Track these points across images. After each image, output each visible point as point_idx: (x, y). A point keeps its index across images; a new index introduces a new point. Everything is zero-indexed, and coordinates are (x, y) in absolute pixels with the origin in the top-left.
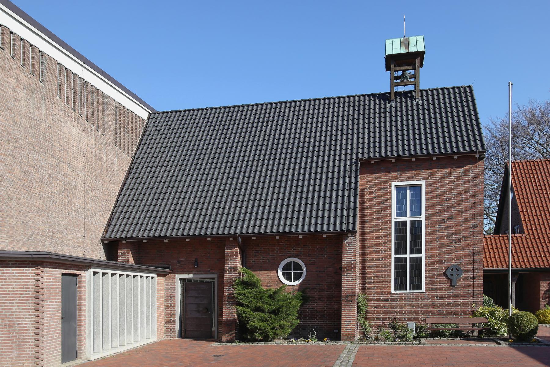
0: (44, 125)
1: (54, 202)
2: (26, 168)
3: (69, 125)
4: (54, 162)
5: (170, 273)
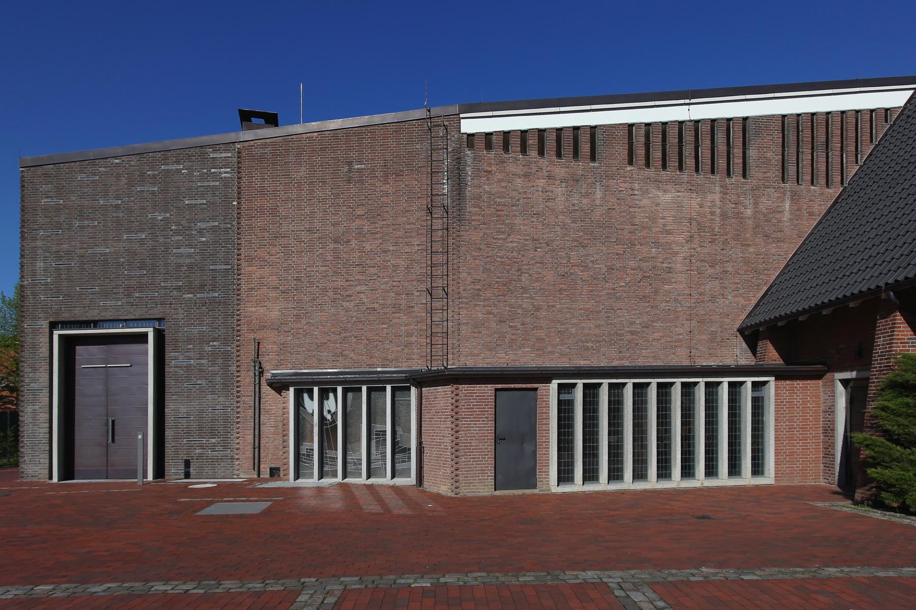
0: (598, 213)
1: (618, 299)
2: (562, 270)
3: (654, 192)
5: (826, 372)
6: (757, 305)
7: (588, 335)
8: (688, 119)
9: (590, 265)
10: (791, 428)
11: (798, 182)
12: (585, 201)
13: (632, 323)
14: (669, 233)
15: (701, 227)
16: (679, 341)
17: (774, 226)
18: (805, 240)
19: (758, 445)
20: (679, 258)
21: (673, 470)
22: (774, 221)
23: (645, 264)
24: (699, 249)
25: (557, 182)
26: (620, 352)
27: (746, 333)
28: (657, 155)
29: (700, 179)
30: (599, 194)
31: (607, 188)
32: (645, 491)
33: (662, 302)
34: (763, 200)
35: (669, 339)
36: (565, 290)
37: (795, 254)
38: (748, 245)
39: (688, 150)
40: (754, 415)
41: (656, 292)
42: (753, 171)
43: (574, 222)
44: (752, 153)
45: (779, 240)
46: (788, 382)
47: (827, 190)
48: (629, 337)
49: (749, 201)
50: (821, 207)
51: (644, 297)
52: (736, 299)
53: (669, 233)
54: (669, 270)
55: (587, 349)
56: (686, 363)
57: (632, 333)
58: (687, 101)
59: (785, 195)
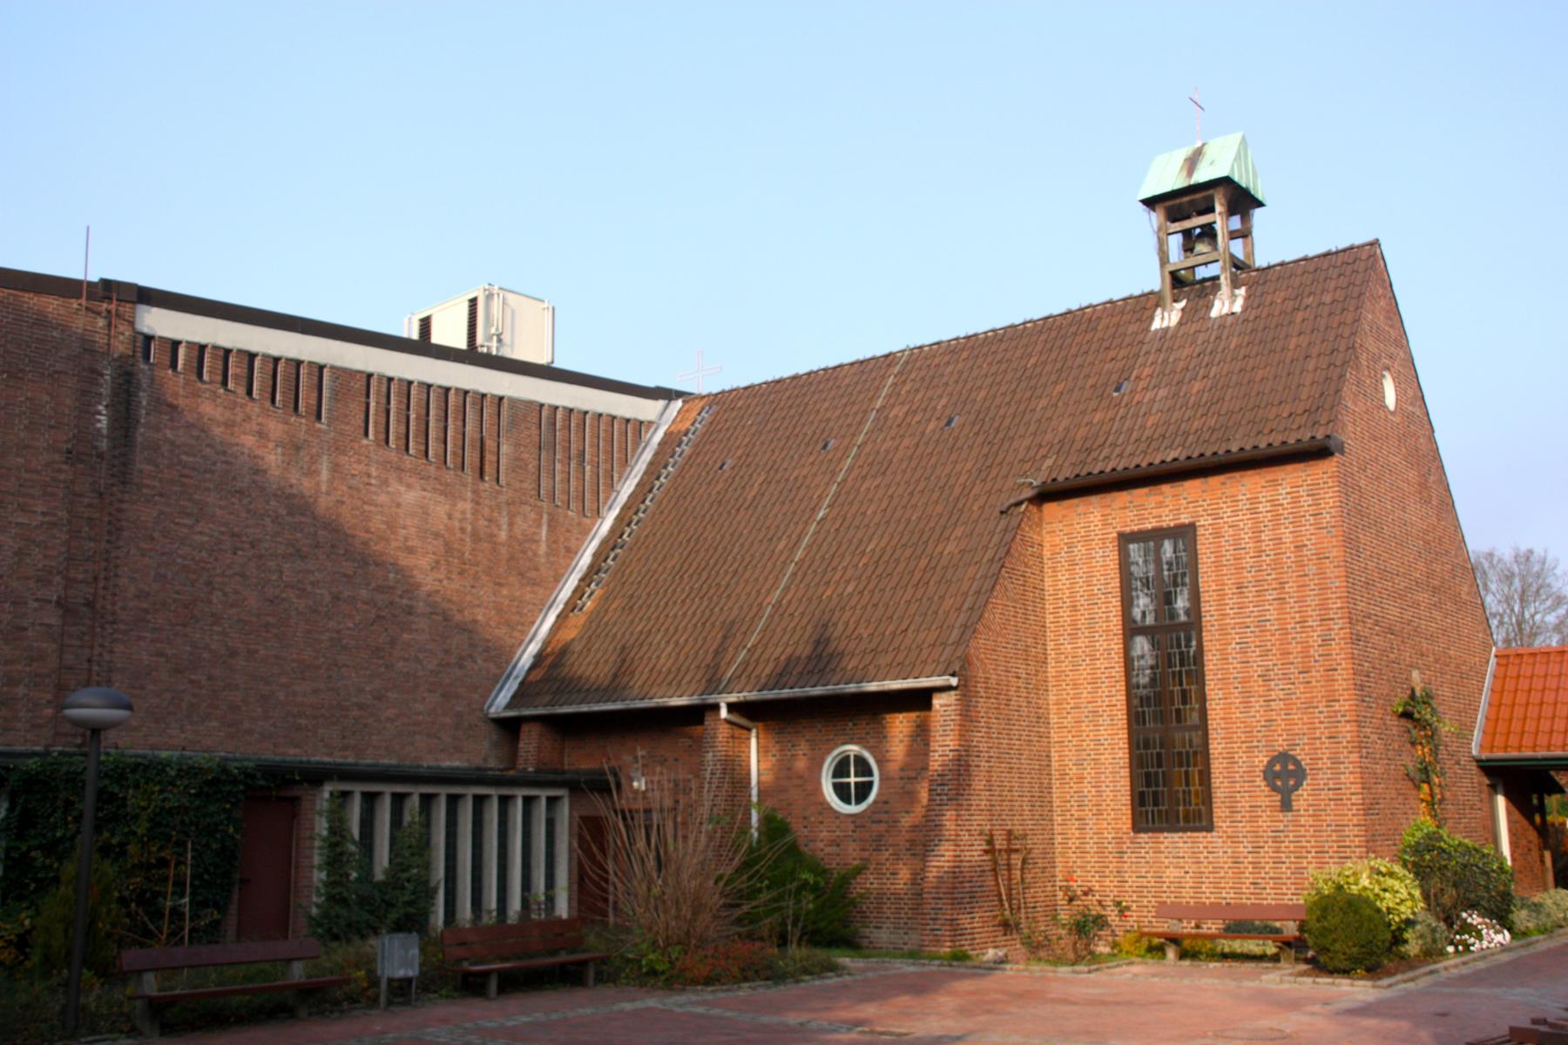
3: (395, 486)
9: (309, 588)
14: (411, 551)
22: (530, 554)
24: (445, 582)
25: (271, 445)
41: (393, 642)
48: (356, 712)
51: (378, 649)
54: (410, 611)
57: (361, 706)
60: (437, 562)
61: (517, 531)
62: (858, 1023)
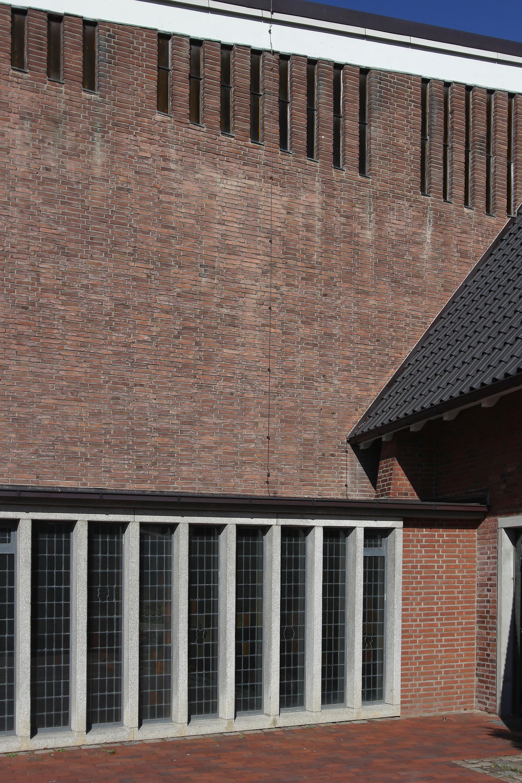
0: (97, 194)
1: (137, 365)
2: (23, 296)
3: (206, 171)
4: (138, 269)
5: (485, 515)
6: (380, 398)
7: (76, 430)
8: (268, 48)
9: (81, 293)
10: (429, 614)
11: (445, 197)
12: (71, 165)
13: (163, 414)
14: (232, 251)
15: (288, 251)
16: (250, 453)
17: (409, 265)
18: (455, 297)
19: (374, 645)
20: (251, 301)
21: (221, 697)
22: (408, 257)
23: (188, 305)
24: (284, 289)
25: (13, 117)
26: (140, 468)
27: (362, 447)
28: (211, 102)
29: (287, 161)
30: (99, 157)
31: (115, 149)
32: (163, 744)
33: (218, 378)
34: (392, 217)
35: (230, 449)
36: (28, 337)
37: (440, 317)
38: (367, 293)
39: (269, 105)
40: (367, 590)
41: (208, 359)
42: (375, 164)
43: (49, 202)
44: (375, 132)
45: (415, 292)
46: (425, 531)
47: (487, 218)
48: (156, 439)
49: (368, 217)
50: (478, 245)
51: (186, 366)
52: (346, 386)
53: (232, 251)
54: (233, 322)
55: (73, 457)
56: (260, 491)
57: (163, 432)
58: (267, 14)
59: (425, 215)
60: (272, 265)
61: (389, 230)
62: (211, 177)
